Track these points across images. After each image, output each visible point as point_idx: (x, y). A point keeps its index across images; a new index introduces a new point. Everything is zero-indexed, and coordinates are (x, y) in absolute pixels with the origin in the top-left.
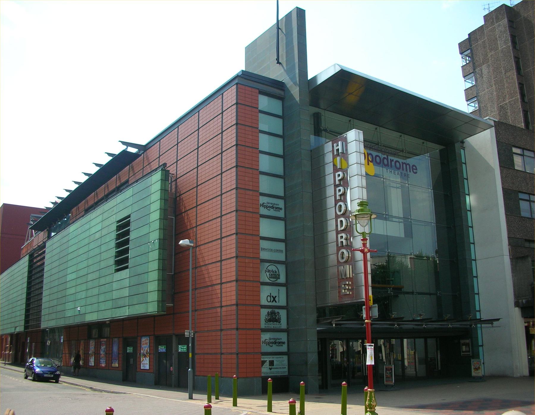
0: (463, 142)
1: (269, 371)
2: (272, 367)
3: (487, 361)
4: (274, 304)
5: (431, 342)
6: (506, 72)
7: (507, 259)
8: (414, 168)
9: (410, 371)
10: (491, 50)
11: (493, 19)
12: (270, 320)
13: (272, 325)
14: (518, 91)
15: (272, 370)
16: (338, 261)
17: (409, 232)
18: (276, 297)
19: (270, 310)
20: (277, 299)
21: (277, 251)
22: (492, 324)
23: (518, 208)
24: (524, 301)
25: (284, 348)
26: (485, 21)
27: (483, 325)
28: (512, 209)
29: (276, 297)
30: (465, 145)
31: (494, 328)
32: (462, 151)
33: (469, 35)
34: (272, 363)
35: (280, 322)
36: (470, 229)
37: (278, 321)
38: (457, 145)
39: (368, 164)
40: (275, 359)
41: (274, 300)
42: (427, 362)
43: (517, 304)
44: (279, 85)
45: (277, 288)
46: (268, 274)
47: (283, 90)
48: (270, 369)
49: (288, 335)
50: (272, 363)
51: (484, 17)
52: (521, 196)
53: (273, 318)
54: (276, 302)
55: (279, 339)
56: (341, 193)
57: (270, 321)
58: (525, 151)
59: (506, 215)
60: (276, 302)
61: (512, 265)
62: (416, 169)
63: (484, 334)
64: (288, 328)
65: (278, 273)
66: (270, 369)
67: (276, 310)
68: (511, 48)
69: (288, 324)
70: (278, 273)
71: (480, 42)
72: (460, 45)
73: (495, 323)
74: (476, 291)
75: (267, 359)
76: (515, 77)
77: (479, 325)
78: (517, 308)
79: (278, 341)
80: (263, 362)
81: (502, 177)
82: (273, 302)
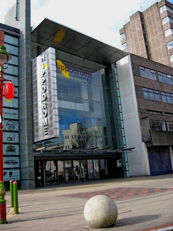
0: (115, 64)
1: (9, 178)
2: (11, 176)
3: (130, 169)
4: (12, 142)
5: (102, 161)
6: (140, 41)
7: (137, 119)
8: (91, 75)
9: (96, 178)
10: (133, 31)
11: (134, 18)
12: (9, 151)
13: (10, 153)
14: (145, 49)
15: (11, 177)
16: (43, 117)
17: (91, 108)
18: (12, 138)
19: (9, 145)
20: (13, 139)
21: (13, 114)
22: (131, 150)
23: (142, 94)
24: (146, 139)
25: (17, 166)
26: (130, 19)
27: (127, 151)
28: (139, 96)
29: (12, 138)
30: (117, 66)
31: (132, 153)
32: (115, 69)
33: (124, 26)
34: (11, 173)
35: (15, 151)
36: (120, 106)
37: (14, 151)
38: (113, 65)
39: (66, 72)
40: (13, 171)
41: (12, 139)
42: (101, 172)
43: (143, 141)
44: (17, 31)
45: (12, 133)
46: (8, 126)
47: (19, 33)
48: (10, 177)
49: (20, 159)
50: (11, 173)
51: (130, 17)
52: (144, 89)
53: (11, 150)
54: (13, 141)
55: (14, 161)
56: (43, 81)
57: (9, 151)
58: (145, 68)
59: (137, 98)
60: (13, 141)
61: (140, 121)
62: (92, 76)
63: (128, 156)
64: (20, 155)
65: (14, 125)
66: (10, 177)
67: (13, 145)
68: (142, 30)
69: (19, 152)
70: (14, 125)
71: (128, 29)
72: (120, 31)
73: (133, 150)
74: (123, 135)
75: (8, 172)
76: (144, 43)
77: (125, 151)
78: (143, 143)
79: (13, 162)
80: (5, 173)
81: (134, 80)
82: (11, 141)
